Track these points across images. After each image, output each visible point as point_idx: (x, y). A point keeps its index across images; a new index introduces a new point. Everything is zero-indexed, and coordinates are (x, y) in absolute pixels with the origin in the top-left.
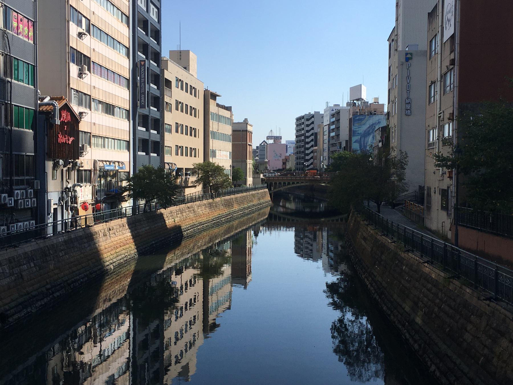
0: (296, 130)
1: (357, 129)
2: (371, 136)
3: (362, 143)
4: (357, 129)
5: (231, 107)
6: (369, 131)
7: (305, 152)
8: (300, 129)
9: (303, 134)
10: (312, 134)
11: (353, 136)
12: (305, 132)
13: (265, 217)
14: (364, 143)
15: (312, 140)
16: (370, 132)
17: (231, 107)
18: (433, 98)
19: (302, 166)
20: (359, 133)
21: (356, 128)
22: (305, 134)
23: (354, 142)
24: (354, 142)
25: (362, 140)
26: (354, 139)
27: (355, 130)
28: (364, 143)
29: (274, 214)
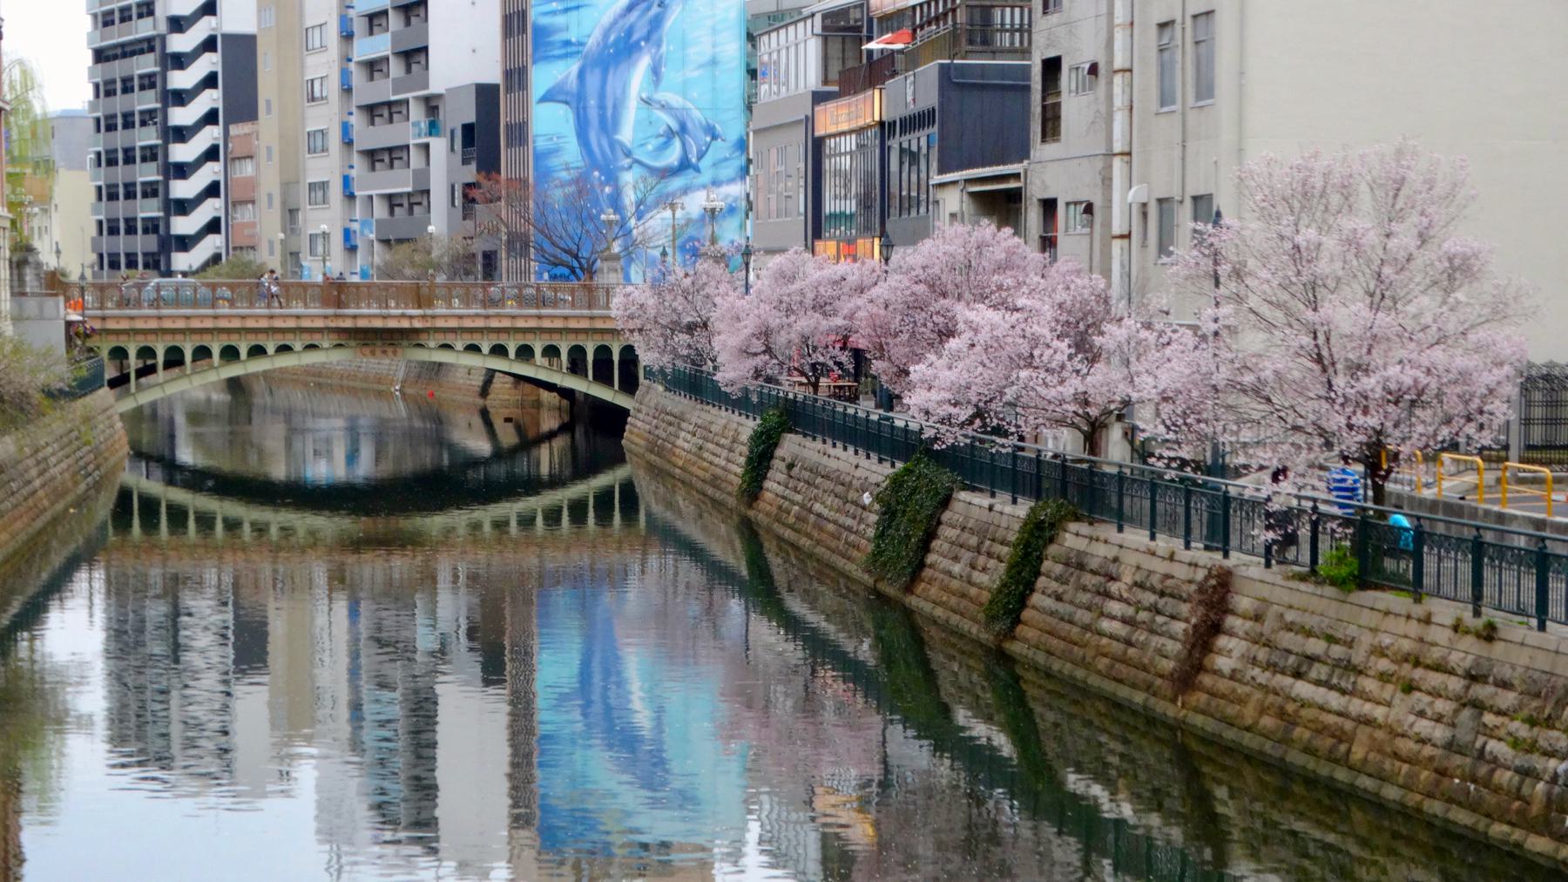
0: (95, 16)
1: (560, 20)
2: (643, 63)
3: (592, 102)
4: (560, 20)
5: (1211, 195)
6: (630, 32)
7: (166, 155)
8: (112, 12)
9: (150, 40)
10: (209, 45)
11: (534, 62)
12: (163, 28)
13: (409, 453)
14: (602, 107)
15: (210, 81)
16: (635, 37)
17: (1211, 195)
18: (1117, 21)
19: (143, 243)
20: (567, 43)
21: (554, 13)
22: (163, 38)
23: (544, 99)
24: (544, 99)
25: (593, 81)
26: (542, 78)
27: (545, 21)
28: (602, 107)
29: (195, 507)
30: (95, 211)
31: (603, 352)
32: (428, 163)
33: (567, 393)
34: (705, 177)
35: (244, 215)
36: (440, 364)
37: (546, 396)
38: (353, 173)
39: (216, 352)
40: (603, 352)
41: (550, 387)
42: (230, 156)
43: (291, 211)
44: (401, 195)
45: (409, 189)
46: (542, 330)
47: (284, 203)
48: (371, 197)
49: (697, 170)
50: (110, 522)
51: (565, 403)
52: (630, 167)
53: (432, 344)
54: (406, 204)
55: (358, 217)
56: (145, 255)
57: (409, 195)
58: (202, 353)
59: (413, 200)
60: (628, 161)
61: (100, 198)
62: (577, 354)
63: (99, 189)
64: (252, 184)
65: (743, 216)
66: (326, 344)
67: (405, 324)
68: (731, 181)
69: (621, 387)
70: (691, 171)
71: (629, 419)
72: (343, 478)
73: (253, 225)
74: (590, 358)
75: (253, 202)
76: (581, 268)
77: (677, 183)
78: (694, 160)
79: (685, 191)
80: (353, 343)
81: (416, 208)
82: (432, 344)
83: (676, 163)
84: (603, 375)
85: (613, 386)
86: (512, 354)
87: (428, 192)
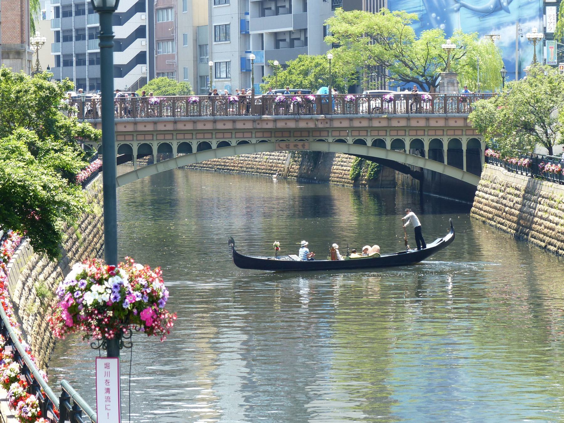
30: (55, 50)
31: (455, 144)
32: (305, 10)
33: (419, 174)
34: (513, 16)
35: (167, 49)
36: (319, 153)
37: (400, 176)
38: (248, 18)
39: (175, 148)
40: (455, 144)
41: (404, 168)
42: (155, 8)
43: (200, 46)
44: (284, 33)
45: (291, 29)
46: (353, 129)
47: (196, 40)
48: (262, 35)
49: (508, 11)
50: (315, 282)
51: (417, 181)
52: (458, 10)
53: (330, 140)
54: (288, 40)
55: (251, 50)
56: (91, 79)
57: (290, 32)
58: (145, 150)
59: (294, 36)
60: (457, 5)
61: (58, 40)
62: (417, 145)
63: (58, 33)
64: (174, 26)
65: (542, 43)
66: (254, 141)
67: (311, 125)
68: (532, 18)
69: (468, 170)
70: (503, 11)
71: (477, 192)
72: (118, 249)
73: (172, 57)
74: (445, 148)
75: (172, 40)
76: (427, 83)
77: (492, 20)
78: (505, 4)
79: (499, 26)
80: (273, 140)
81: (281, 43)
82: (330, 140)
83: (492, 6)
84: (455, 162)
85: (462, 169)
86: (388, 146)
87: (305, 30)
